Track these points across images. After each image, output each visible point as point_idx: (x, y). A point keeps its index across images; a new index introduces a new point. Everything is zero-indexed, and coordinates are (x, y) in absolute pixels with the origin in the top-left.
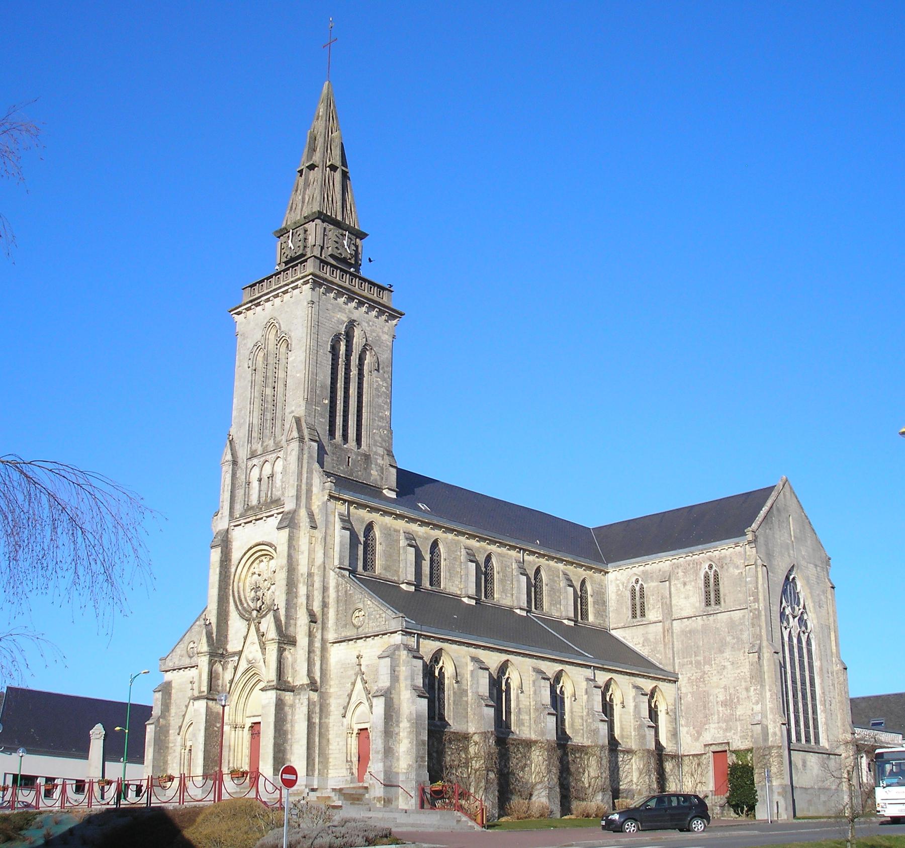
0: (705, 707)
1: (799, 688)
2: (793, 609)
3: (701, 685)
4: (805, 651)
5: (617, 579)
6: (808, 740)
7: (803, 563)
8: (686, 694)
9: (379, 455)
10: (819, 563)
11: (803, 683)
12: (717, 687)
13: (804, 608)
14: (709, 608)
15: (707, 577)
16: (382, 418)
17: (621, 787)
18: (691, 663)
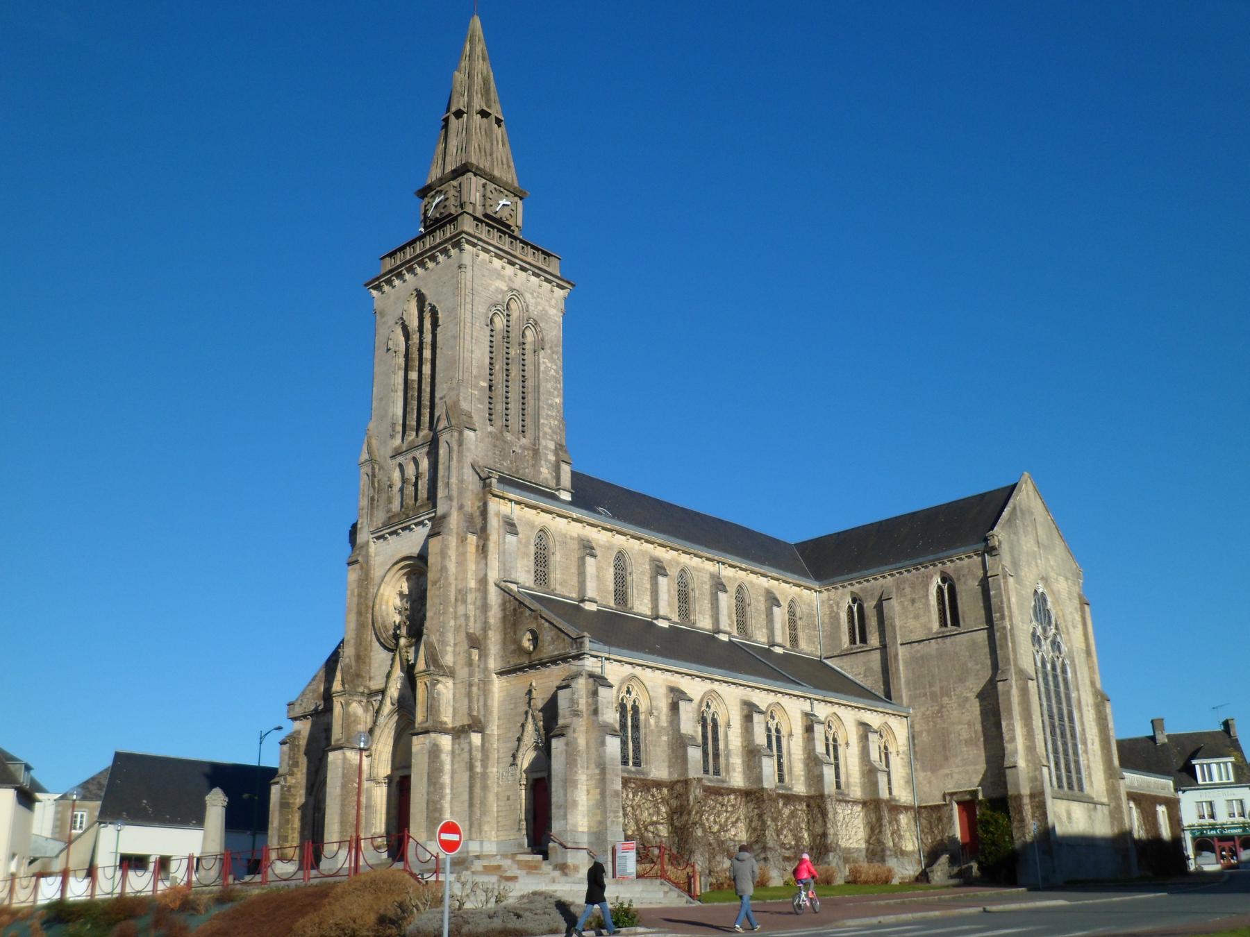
0: (944, 747)
2: (1045, 630)
3: (939, 720)
4: (1060, 679)
5: (829, 599)
6: (1071, 787)
7: (1053, 574)
8: (921, 732)
9: (550, 449)
10: (1069, 575)
11: (1061, 718)
12: (960, 723)
14: (944, 629)
15: (940, 589)
16: (551, 405)
18: (925, 695)
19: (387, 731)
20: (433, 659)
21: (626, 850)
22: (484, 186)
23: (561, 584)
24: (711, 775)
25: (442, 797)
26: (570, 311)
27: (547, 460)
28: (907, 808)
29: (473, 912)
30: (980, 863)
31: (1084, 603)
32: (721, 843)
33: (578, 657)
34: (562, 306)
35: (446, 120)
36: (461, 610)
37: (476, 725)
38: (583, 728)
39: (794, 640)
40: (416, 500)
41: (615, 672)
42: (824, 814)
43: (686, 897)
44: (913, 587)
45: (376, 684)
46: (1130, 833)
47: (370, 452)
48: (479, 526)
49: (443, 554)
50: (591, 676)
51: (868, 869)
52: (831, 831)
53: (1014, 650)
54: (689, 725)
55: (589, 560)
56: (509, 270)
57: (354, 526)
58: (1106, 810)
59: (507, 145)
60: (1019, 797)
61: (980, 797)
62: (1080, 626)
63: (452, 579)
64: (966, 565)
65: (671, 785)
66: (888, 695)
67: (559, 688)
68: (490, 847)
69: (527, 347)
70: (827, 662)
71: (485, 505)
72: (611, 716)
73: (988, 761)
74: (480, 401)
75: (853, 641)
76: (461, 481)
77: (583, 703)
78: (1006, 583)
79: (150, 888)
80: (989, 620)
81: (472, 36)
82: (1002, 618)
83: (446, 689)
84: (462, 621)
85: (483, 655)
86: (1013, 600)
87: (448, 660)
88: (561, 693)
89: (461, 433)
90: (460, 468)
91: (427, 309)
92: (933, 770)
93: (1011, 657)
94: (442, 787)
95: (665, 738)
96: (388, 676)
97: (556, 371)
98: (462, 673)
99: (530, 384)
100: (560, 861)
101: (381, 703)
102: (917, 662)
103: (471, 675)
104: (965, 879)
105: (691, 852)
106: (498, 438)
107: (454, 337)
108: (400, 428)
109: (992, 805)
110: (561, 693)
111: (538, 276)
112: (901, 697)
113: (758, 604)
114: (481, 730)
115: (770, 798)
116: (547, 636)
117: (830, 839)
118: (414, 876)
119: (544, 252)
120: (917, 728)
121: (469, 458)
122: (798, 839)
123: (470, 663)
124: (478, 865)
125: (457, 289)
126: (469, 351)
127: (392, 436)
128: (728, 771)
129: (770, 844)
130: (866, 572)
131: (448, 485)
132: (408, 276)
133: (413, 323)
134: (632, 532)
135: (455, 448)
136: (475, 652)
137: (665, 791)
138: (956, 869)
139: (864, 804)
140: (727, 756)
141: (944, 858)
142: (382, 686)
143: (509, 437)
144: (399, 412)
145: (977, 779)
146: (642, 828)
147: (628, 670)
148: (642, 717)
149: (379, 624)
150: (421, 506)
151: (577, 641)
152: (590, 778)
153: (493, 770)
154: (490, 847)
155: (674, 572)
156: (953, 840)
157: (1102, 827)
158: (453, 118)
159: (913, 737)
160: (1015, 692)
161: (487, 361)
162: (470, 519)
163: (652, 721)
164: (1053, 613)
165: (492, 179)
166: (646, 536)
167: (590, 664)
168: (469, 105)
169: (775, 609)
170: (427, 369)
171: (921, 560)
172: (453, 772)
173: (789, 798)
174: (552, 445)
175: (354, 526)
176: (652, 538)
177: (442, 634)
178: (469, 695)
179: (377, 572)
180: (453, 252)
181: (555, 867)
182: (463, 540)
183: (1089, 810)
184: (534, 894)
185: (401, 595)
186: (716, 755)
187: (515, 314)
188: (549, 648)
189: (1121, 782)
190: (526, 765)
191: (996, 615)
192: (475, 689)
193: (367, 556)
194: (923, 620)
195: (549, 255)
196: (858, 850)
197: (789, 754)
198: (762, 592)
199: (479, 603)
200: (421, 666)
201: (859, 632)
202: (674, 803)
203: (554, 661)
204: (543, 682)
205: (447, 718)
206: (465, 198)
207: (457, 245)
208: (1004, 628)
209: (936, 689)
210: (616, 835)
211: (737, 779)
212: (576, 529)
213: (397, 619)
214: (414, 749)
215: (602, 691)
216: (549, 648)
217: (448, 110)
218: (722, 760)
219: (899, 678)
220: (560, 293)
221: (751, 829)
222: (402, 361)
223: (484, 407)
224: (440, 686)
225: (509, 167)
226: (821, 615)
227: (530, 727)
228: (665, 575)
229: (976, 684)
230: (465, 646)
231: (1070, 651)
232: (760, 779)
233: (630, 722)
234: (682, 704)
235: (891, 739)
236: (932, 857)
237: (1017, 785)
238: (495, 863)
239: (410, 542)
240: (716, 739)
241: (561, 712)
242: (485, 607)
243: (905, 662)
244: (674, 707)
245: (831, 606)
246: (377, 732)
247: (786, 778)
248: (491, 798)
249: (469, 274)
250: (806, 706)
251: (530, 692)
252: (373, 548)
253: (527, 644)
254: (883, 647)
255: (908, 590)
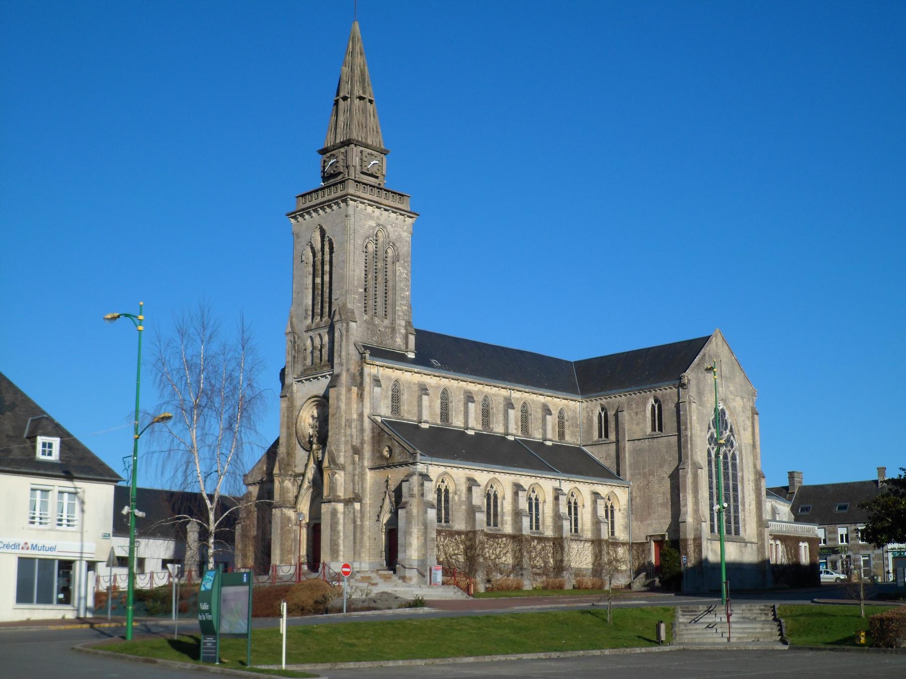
1: (715, 493)
7: (731, 396)
12: (658, 493)
13: (731, 431)
16: (403, 297)
17: (785, 561)
19: (305, 498)
20: (333, 461)
21: (437, 569)
22: (361, 152)
23: (408, 413)
24: (492, 527)
25: (338, 538)
26: (416, 232)
27: (400, 333)
28: (624, 544)
29: (356, 600)
30: (660, 578)
31: (754, 412)
32: (496, 565)
33: (414, 464)
34: (411, 230)
35: (336, 103)
36: (348, 431)
37: (357, 498)
38: (416, 504)
39: (562, 435)
40: (321, 360)
41: (435, 470)
42: (562, 548)
43: (466, 595)
44: (637, 404)
45: (299, 469)
46: (769, 561)
47: (292, 327)
48: (359, 382)
49: (338, 398)
50: (421, 474)
51: (588, 581)
52: (566, 559)
53: (691, 450)
54: (478, 499)
55: (425, 398)
56: (377, 211)
57: (283, 371)
58: (755, 547)
59: (377, 116)
60: (686, 540)
61: (667, 538)
62: (750, 429)
63: (343, 413)
64: (668, 392)
65: (467, 534)
66: (618, 474)
67: (403, 481)
68: (365, 566)
69: (388, 259)
70: (584, 448)
71: (362, 369)
72: (432, 497)
73: (672, 518)
74: (359, 301)
75: (600, 436)
76: (348, 354)
77: (416, 490)
78: (690, 407)
79: (149, 585)
80: (679, 430)
81: (353, 38)
82: (686, 429)
83: (340, 477)
84: (349, 438)
85: (361, 459)
86: (694, 418)
87: (341, 460)
88: (404, 484)
89: (348, 324)
90: (347, 346)
91: (326, 239)
92: (641, 522)
93: (690, 454)
94: (338, 532)
95: (464, 507)
96: (306, 465)
97: (407, 274)
98: (349, 468)
99: (390, 284)
100: (402, 575)
101: (302, 481)
102: (637, 452)
103: (354, 469)
104: (651, 588)
105: (476, 571)
106: (370, 323)
107: (343, 261)
108: (310, 313)
109: (672, 543)
110: (404, 484)
111: (395, 213)
112: (625, 475)
113: (536, 414)
114: (360, 501)
115: (527, 540)
116: (397, 450)
117: (565, 563)
118: (328, 583)
119: (399, 194)
120: (634, 494)
121: (353, 339)
122: (546, 563)
123: (354, 463)
124: (358, 576)
125: (345, 229)
126: (352, 269)
127: (306, 318)
128: (502, 525)
129: (525, 566)
130: (609, 392)
131: (340, 356)
132: (314, 214)
133: (318, 246)
134: (452, 376)
135: (344, 333)
136: (356, 457)
137: (463, 537)
138: (648, 581)
139: (593, 542)
140: (502, 516)
141: (643, 574)
142: (303, 471)
143: (377, 321)
144: (310, 302)
145: (666, 527)
146: (448, 556)
147: (442, 469)
148: (451, 496)
149: (300, 434)
150: (324, 366)
151: (413, 455)
152: (419, 530)
153: (367, 523)
154: (365, 566)
155: (479, 399)
156: (650, 563)
157: (749, 556)
158: (341, 100)
159: (631, 500)
160: (690, 477)
161: (363, 275)
162: (353, 377)
163: (456, 498)
164: (729, 421)
165: (367, 146)
166: (462, 378)
167: (420, 468)
168: (351, 92)
169: (548, 417)
170: (327, 278)
171: (643, 387)
172: (344, 524)
173: (541, 539)
174: (403, 323)
175: (283, 371)
176: (466, 379)
177: (338, 446)
178: (353, 481)
179: (298, 403)
180: (342, 205)
181: (399, 578)
182: (349, 390)
183: (741, 547)
184: (383, 592)
185: (312, 416)
186: (496, 515)
187: (381, 240)
188: (398, 458)
189: (766, 529)
190: (385, 521)
191: (683, 427)
192: (356, 477)
193: (292, 393)
194: (641, 426)
195: (402, 195)
196: (587, 569)
197: (543, 513)
198: (540, 406)
199: (359, 427)
200: (326, 464)
201: (604, 431)
202: (468, 543)
203: (401, 465)
204: (395, 475)
205: (341, 493)
206: (349, 163)
207: (345, 201)
208: (687, 436)
209: (646, 471)
210: (432, 561)
211: (508, 529)
212: (417, 378)
213: (311, 431)
214: (322, 511)
215: (426, 484)
216: (398, 458)
217: (338, 95)
218: (499, 518)
219: (625, 462)
220: (409, 221)
221: (515, 557)
222: (311, 269)
223: (361, 305)
224: (337, 476)
225: (377, 132)
226: (582, 418)
227: (387, 500)
228: (473, 402)
229: (668, 470)
230: (350, 453)
231: (740, 446)
232: (521, 529)
233: (443, 495)
234: (474, 488)
235: (615, 501)
236: (637, 573)
237: (685, 534)
238: (367, 575)
239: (319, 386)
240: (496, 506)
241: (404, 494)
242: (362, 430)
243: (630, 452)
244: (470, 490)
245: (588, 412)
246: (300, 498)
247: (541, 527)
248: (366, 538)
249: (352, 220)
250: (556, 484)
251: (387, 481)
252: (295, 387)
253: (386, 453)
254: (617, 442)
255: (634, 406)
